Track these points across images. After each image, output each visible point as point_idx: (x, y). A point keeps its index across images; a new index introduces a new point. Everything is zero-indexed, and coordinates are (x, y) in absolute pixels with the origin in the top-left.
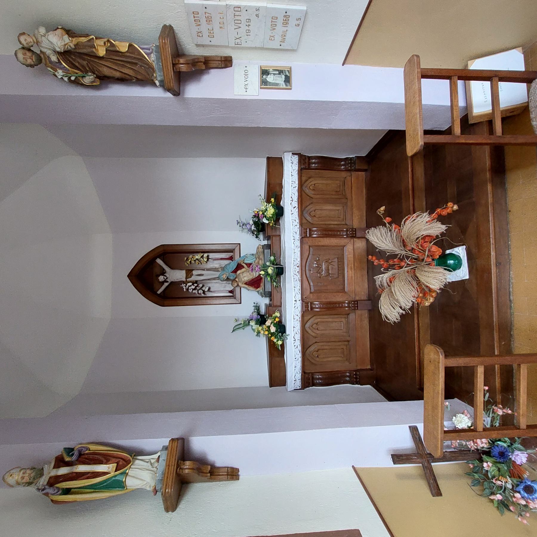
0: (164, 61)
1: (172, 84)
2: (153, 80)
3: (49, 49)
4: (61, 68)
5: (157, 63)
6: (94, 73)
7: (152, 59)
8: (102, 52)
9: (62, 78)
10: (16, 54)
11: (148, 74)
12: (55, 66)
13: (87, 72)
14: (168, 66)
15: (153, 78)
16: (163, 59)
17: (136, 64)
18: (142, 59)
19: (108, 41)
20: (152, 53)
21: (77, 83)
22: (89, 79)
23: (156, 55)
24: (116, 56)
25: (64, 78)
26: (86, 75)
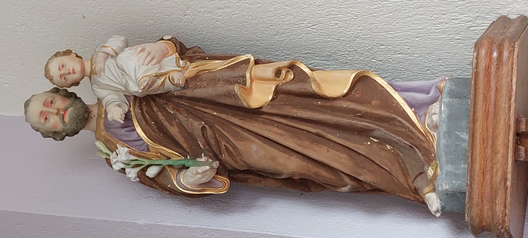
0: (479, 125)
1: (499, 208)
2: (416, 191)
3: (117, 91)
4: (126, 143)
5: (449, 133)
6: (216, 157)
7: (434, 121)
8: (260, 96)
9: (123, 170)
10: (27, 104)
11: (405, 173)
12: (111, 134)
13: (196, 155)
14: (494, 139)
15: (418, 183)
16: (480, 114)
17: (365, 133)
18: (392, 117)
19: (292, 67)
20: (433, 101)
21: (158, 186)
22: (196, 174)
23: (449, 106)
24: (305, 108)
25: (127, 170)
26: (190, 163)
